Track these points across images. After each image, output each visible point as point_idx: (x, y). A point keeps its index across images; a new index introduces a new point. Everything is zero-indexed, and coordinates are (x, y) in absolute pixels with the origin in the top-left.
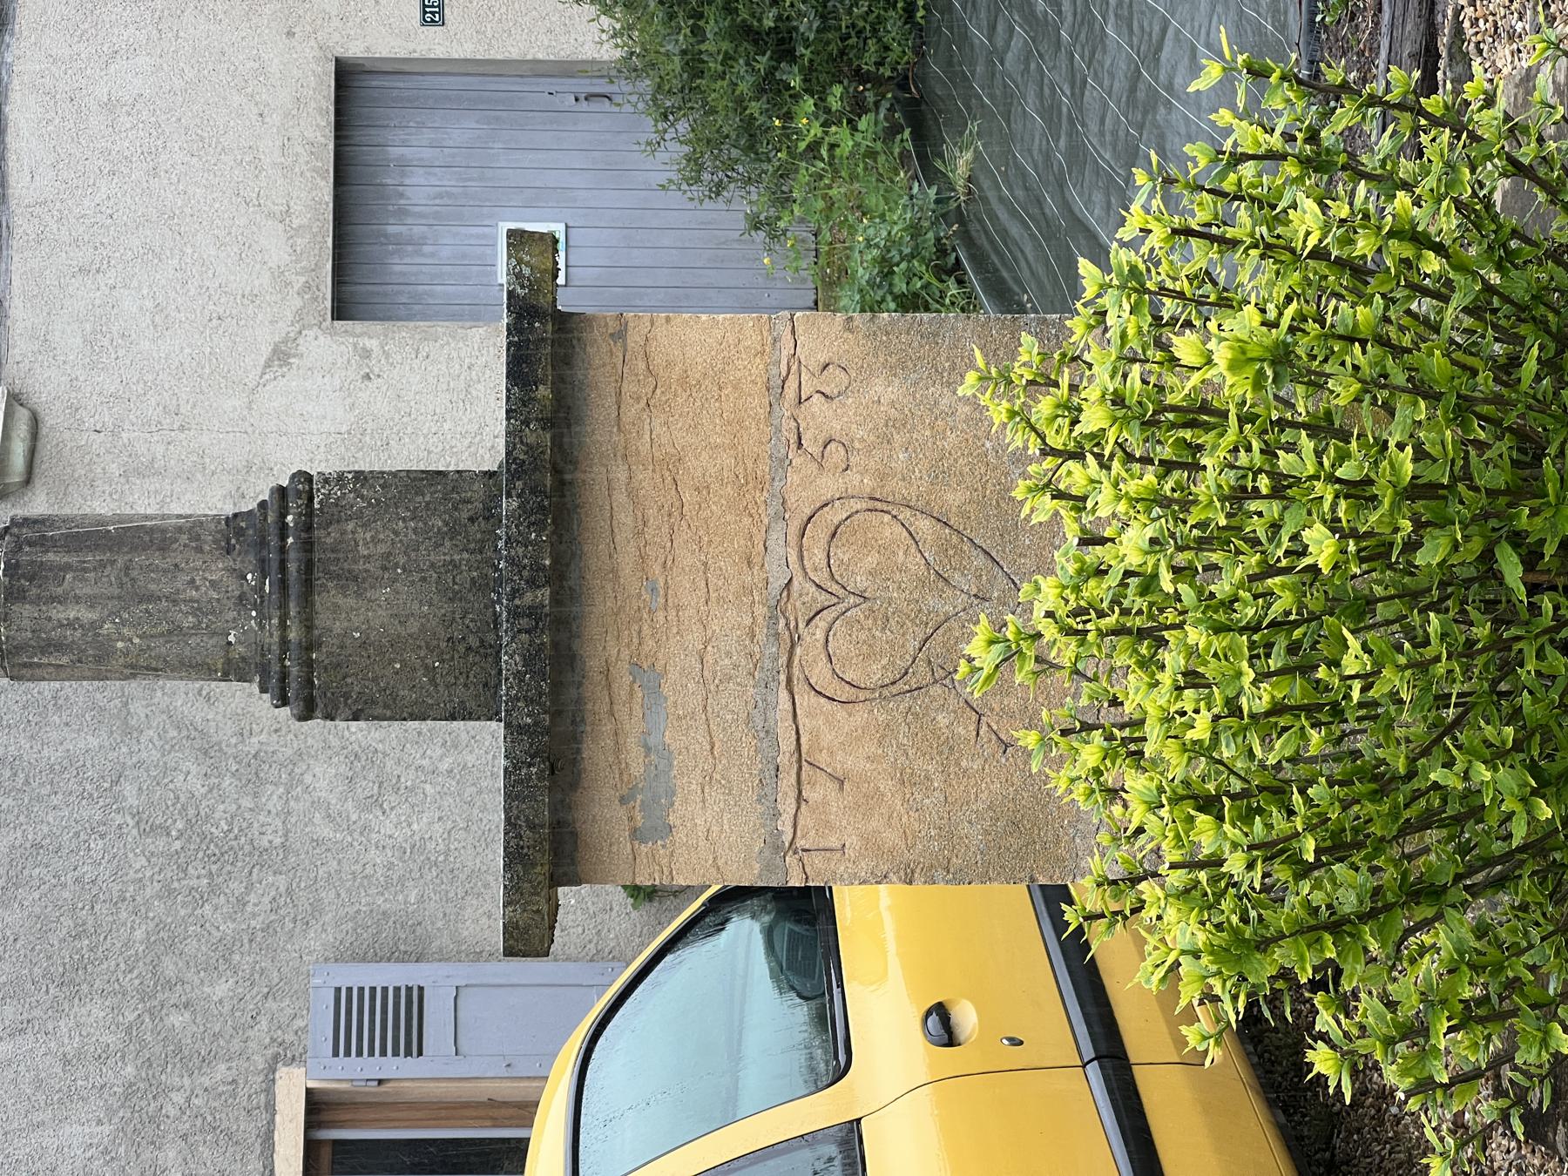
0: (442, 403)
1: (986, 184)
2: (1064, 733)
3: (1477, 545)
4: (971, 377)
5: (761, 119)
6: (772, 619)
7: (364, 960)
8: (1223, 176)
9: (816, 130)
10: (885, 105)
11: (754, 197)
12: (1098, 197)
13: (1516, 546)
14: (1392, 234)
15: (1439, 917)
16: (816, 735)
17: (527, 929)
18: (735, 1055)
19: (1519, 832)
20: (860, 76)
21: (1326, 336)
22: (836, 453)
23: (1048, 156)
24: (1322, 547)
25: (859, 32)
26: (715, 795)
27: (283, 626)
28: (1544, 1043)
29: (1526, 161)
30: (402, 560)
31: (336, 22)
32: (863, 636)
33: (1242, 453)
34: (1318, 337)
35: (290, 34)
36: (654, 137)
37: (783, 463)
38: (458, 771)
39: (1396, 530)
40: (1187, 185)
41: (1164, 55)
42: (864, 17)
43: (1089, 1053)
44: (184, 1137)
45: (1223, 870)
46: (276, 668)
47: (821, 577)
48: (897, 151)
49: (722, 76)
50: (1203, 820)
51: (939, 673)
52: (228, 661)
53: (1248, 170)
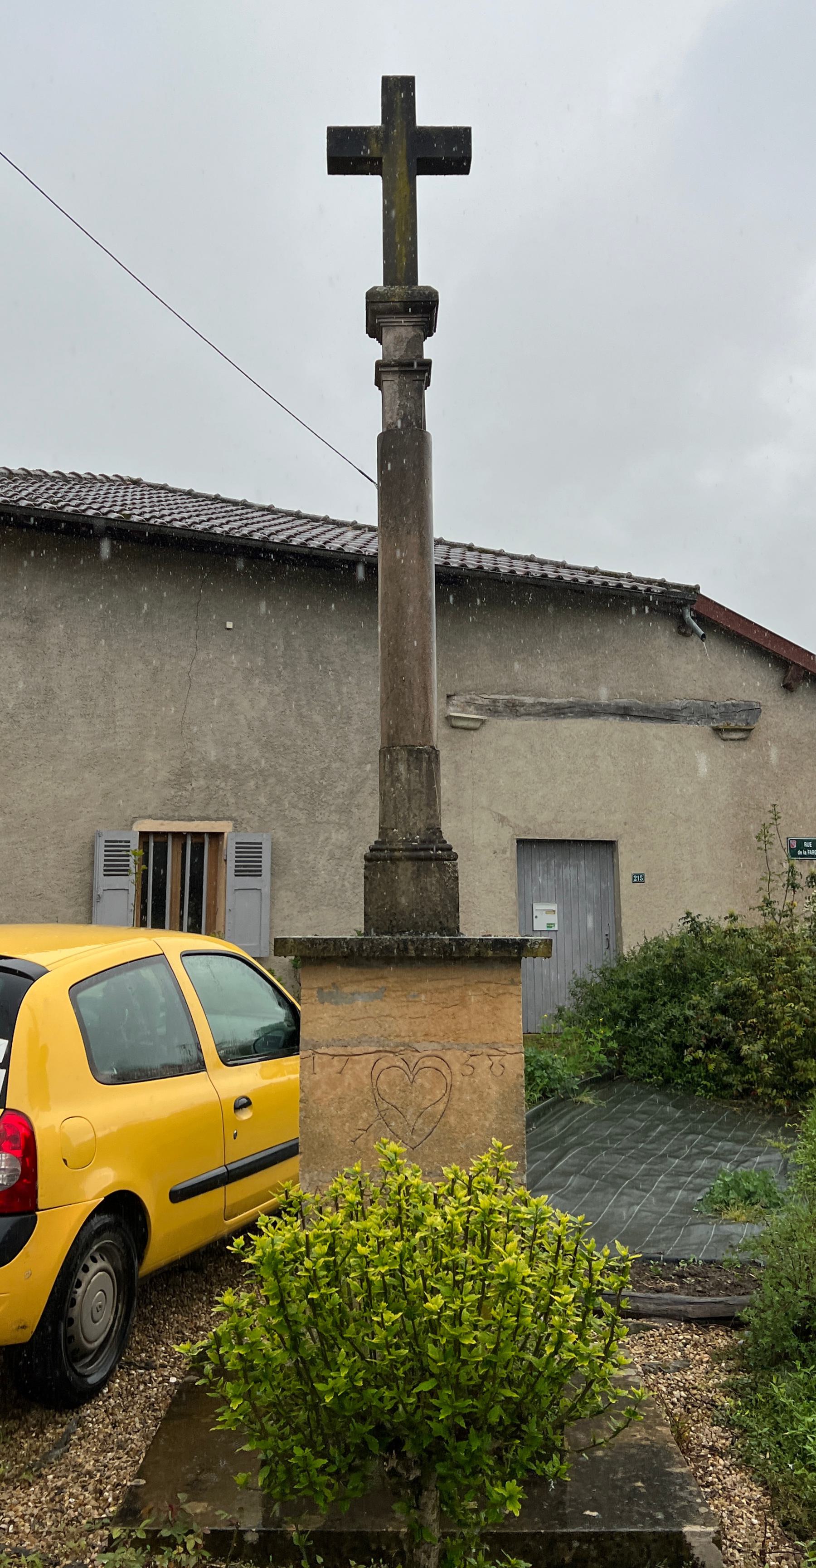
0: (486, 909)
1: (580, 1110)
2: (360, 1182)
3: (436, 1371)
4: (500, 1144)
5: (603, 1013)
6: (404, 1044)
7: (272, 853)
8: (583, 1255)
9: (599, 1037)
10: (611, 1065)
11: (571, 1009)
12: (577, 1161)
13: (436, 1386)
14: (560, 1333)
15: (286, 1349)
16: (359, 1062)
17: (285, 947)
18: (235, 1013)
19: (320, 1387)
20: (622, 1053)
21: (519, 1304)
22: (469, 1071)
23: (591, 1138)
24: (435, 1303)
25: (639, 1054)
26: (335, 1021)
27: (399, 850)
28: (235, 1396)
29: (593, 1387)
30: (425, 895)
31: (631, 841)
32: (397, 1082)
33: (472, 1267)
34: (519, 1301)
35: (625, 824)
36: (593, 968)
37: (465, 1049)
38: (347, 923)
39: (442, 1336)
40: (578, 1238)
41: (635, 1191)
42: (645, 1056)
43: (230, 1168)
44: (208, 787)
45: (305, 1258)
46: (384, 847)
47: (420, 1064)
48: (592, 1070)
49: (619, 997)
50: (325, 1248)
51: (383, 1113)
52: (386, 829)
53: (586, 1264)
